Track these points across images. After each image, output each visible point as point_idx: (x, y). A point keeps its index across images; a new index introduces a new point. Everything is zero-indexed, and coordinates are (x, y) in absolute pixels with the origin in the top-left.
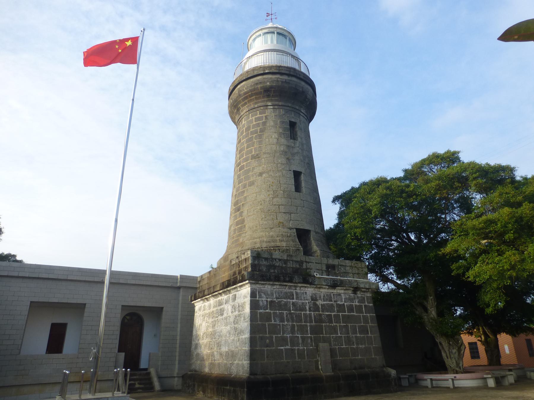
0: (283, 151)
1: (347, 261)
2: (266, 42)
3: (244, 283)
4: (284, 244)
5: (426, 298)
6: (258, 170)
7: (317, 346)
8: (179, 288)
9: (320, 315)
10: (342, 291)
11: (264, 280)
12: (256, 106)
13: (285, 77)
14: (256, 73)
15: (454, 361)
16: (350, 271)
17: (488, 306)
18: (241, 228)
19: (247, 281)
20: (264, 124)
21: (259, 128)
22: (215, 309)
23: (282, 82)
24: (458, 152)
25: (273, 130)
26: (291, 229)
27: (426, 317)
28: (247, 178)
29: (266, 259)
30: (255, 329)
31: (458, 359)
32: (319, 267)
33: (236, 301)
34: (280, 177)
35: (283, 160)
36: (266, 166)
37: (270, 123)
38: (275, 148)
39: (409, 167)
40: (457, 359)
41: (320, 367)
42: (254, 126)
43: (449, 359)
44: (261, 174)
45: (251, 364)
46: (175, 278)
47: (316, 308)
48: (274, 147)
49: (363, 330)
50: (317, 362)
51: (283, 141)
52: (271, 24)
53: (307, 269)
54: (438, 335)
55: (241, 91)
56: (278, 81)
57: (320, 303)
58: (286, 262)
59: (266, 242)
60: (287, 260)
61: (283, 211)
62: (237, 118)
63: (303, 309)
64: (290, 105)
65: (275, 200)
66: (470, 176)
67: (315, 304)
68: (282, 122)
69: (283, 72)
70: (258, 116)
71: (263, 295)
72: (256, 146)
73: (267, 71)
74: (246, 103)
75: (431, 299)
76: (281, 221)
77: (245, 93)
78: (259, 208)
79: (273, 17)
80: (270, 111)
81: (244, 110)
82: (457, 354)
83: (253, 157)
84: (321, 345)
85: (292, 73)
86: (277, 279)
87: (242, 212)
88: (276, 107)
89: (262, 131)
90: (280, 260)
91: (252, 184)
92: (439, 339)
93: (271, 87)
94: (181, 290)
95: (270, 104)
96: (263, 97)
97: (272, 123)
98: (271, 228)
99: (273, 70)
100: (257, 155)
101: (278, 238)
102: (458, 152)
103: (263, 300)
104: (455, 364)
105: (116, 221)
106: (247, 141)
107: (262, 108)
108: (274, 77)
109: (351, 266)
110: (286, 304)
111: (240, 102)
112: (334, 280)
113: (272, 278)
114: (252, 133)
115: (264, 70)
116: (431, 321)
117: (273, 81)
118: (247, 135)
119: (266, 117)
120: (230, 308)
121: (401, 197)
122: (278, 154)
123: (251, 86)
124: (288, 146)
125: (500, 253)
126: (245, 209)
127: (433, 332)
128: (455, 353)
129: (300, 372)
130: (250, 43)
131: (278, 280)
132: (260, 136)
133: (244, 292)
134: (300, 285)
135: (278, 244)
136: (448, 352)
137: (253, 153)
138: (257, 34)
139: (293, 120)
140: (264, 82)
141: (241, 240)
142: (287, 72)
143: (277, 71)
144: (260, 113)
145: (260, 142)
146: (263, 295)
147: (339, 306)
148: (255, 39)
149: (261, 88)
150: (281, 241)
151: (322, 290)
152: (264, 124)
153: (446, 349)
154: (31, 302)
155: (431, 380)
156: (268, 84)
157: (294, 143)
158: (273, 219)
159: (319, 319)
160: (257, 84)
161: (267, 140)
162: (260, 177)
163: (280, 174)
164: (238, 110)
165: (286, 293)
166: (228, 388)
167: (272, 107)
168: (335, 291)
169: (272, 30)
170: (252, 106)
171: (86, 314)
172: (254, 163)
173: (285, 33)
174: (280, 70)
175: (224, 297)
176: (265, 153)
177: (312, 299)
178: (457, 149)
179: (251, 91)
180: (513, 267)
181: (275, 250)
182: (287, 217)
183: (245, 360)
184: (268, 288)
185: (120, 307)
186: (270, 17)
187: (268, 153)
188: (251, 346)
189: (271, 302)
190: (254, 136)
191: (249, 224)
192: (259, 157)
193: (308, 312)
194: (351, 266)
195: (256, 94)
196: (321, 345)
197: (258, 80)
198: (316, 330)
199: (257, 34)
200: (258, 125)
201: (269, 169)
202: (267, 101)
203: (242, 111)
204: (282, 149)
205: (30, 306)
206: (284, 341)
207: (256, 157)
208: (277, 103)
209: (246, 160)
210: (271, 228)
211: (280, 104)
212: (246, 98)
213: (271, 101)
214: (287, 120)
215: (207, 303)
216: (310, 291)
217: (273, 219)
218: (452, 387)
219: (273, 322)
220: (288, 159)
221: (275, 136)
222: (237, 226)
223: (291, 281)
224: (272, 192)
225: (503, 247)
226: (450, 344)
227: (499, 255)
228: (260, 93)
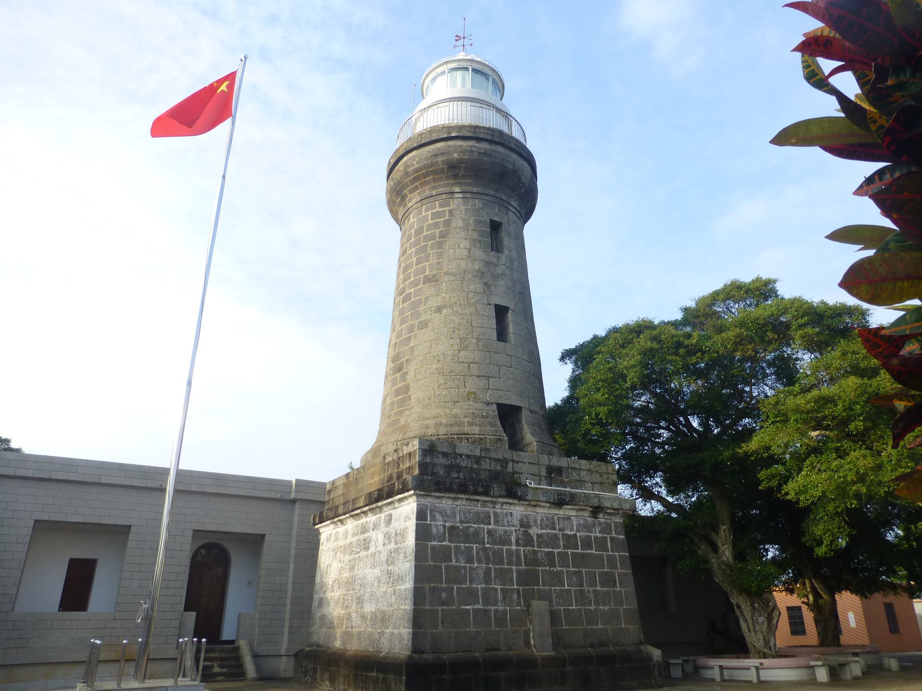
0: (478, 271)
1: (583, 462)
2: (454, 84)
3: (406, 494)
4: (476, 430)
6: (434, 303)
7: (528, 605)
8: (293, 501)
9: (535, 552)
10: (574, 513)
11: (440, 491)
12: (434, 193)
13: (484, 146)
14: (435, 136)
16: (588, 478)
17: (820, 543)
18: (402, 403)
19: (412, 492)
20: (447, 223)
21: (438, 231)
22: (355, 539)
23: (480, 153)
24: (775, 281)
25: (462, 234)
26: (488, 404)
28: (416, 315)
29: (445, 455)
32: (534, 469)
33: (392, 526)
34: (471, 314)
35: (477, 286)
36: (448, 296)
37: (458, 222)
38: (464, 266)
39: (692, 304)
41: (532, 642)
42: (430, 227)
44: (439, 309)
45: (414, 634)
47: (527, 540)
48: (463, 264)
49: (608, 580)
50: (527, 633)
51: (478, 253)
52: (463, 53)
53: (514, 473)
55: (409, 166)
56: (471, 151)
57: (534, 531)
58: (478, 460)
59: (446, 426)
60: (481, 457)
61: (476, 373)
64: (492, 192)
65: (462, 354)
66: (794, 323)
67: (526, 534)
68: (478, 222)
69: (481, 136)
70: (437, 209)
71: (438, 516)
73: (453, 135)
74: (416, 188)
76: (473, 390)
77: (416, 171)
78: (434, 366)
79: (467, 42)
81: (414, 199)
83: (427, 280)
84: (535, 603)
85: (496, 139)
86: (462, 489)
87: (406, 373)
88: (468, 195)
89: (443, 235)
90: (468, 457)
91: (423, 325)
93: (461, 161)
94: (297, 505)
95: (457, 190)
96: (447, 178)
97: (460, 223)
100: (434, 276)
101: (466, 420)
102: (775, 281)
103: (438, 525)
104: (762, 641)
105: (189, 383)
107: (444, 196)
109: (589, 471)
111: (406, 185)
112: (560, 494)
113: (455, 486)
114: (426, 239)
115: (449, 133)
117: (463, 152)
118: (417, 242)
119: (450, 211)
120: (380, 537)
123: (427, 158)
124: (487, 263)
125: (841, 454)
126: (411, 369)
129: (498, 649)
131: (465, 492)
132: (440, 245)
133: (406, 510)
134: (501, 500)
135: (467, 429)
137: (427, 273)
139: (496, 219)
140: (449, 153)
141: (403, 421)
142: (489, 137)
143: (471, 135)
144: (441, 206)
145: (440, 255)
146: (438, 516)
148: (434, 79)
149: (444, 162)
150: (471, 424)
152: (447, 223)
154: (36, 521)
155: (721, 668)
156: (456, 155)
157: (498, 258)
159: (533, 560)
160: (436, 155)
161: (451, 251)
162: (437, 315)
163: (472, 309)
164: (403, 198)
165: (478, 513)
166: (374, 674)
167: (460, 195)
168: (561, 512)
169: (464, 64)
171: (130, 544)
172: (429, 290)
173: (486, 70)
174: (476, 132)
175: (371, 518)
176: (446, 274)
177: (522, 525)
179: (426, 166)
180: (861, 478)
181: (461, 439)
182: (482, 383)
183: (404, 628)
184: (446, 503)
185: (190, 533)
186: (461, 42)
187: (452, 274)
188: (415, 603)
189: (452, 528)
190: (429, 243)
191: (417, 393)
192: (436, 281)
193: (514, 547)
194: (589, 471)
195: (435, 172)
196: (535, 603)
197: (439, 149)
198: (528, 578)
200: (436, 225)
201: (453, 301)
202: (453, 185)
203: (410, 201)
204: (477, 267)
205: (193, 537)
206: (471, 595)
208: (470, 189)
209: (415, 284)
212: (416, 179)
213: (460, 184)
214: (486, 218)
215: (341, 529)
216: (518, 510)
217: (458, 387)
218: (755, 680)
219: (454, 563)
220: (486, 284)
221: (465, 244)
222: (396, 396)
223: (486, 493)
224: (458, 341)
225: (846, 444)
227: (840, 457)
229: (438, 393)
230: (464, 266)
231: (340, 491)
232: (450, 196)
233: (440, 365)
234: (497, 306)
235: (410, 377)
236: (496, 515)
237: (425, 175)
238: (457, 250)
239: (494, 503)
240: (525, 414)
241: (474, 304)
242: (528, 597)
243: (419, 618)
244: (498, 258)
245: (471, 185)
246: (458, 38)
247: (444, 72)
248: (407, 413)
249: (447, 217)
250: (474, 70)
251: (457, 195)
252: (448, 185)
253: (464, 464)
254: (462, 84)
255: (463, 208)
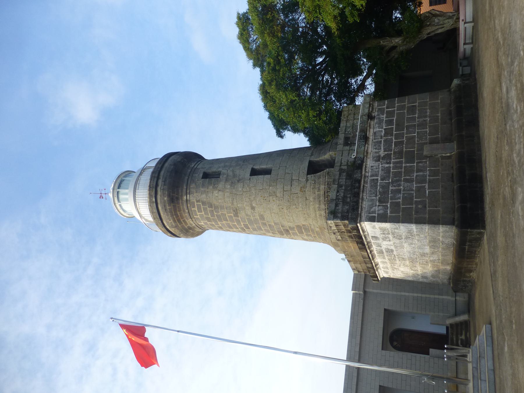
1: (342, 125)
2: (127, 200)
3: (360, 228)
5: (382, 48)
6: (249, 211)
7: (426, 157)
8: (365, 292)
9: (395, 153)
10: (372, 130)
12: (187, 211)
13: (160, 182)
15: (447, 21)
16: (351, 122)
18: (307, 230)
19: (358, 225)
20: (204, 203)
23: (164, 185)
24: (238, 14)
25: (210, 195)
26: (307, 180)
27: (401, 48)
29: (337, 205)
30: (407, 219)
31: (444, 17)
32: (345, 153)
33: (379, 236)
34: (255, 190)
35: (240, 186)
36: (245, 203)
37: (203, 197)
38: (228, 194)
39: (251, 62)
40: (445, 18)
41: (448, 155)
42: (206, 213)
43: (445, 25)
44: (253, 208)
45: (443, 224)
46: (355, 297)
47: (387, 158)
48: (227, 194)
49: (412, 110)
50: (443, 158)
51: (221, 185)
53: (347, 165)
54: (419, 36)
56: (163, 189)
57: (382, 153)
58: (340, 186)
59: (320, 204)
60: (338, 184)
61: (289, 187)
62: (198, 230)
63: (388, 170)
64: (186, 178)
65: (278, 195)
67: (384, 158)
68: (203, 185)
69: (155, 184)
70: (196, 209)
71: (372, 210)
72: (225, 212)
73: (154, 200)
74: (184, 221)
75: (383, 42)
76: (299, 189)
77: (174, 221)
79: (103, 192)
80: (192, 198)
81: (190, 222)
82: (439, 18)
83: (236, 215)
85: (156, 175)
86: (357, 195)
87: (290, 227)
88: (188, 191)
89: (211, 206)
90: (338, 192)
91: (262, 217)
92: (424, 35)
93: (169, 196)
94: (367, 290)
95: (185, 197)
96: (178, 203)
97: (204, 196)
98: (306, 199)
99: (153, 193)
100: (234, 211)
101: (317, 193)
102: (238, 14)
103: (378, 209)
104: (450, 20)
106: (220, 220)
107: (189, 205)
108: (159, 193)
110: (382, 187)
111: (183, 226)
112: (360, 138)
113: (355, 200)
114: (213, 215)
115: (153, 202)
116: (405, 43)
117: (164, 194)
119: (198, 201)
121: (279, 71)
122: (234, 190)
123: (167, 215)
124: (227, 180)
126: (287, 224)
127: (417, 41)
128: (439, 19)
129: (453, 174)
130: (128, 216)
131: (358, 194)
132: (216, 208)
133: (369, 228)
134: (363, 173)
135: (322, 193)
136: (437, 27)
138: (119, 208)
139: (201, 175)
140: (164, 202)
141: (318, 229)
143: (154, 190)
144: (194, 207)
145: (222, 208)
146: (372, 210)
147: (386, 134)
149: (169, 205)
150: (319, 190)
151: (370, 151)
152: (204, 203)
153: (434, 28)
156: (166, 199)
157: (224, 174)
158: (298, 197)
159: (399, 154)
160: (166, 210)
161: (220, 201)
163: (253, 189)
164: (190, 228)
166: (467, 247)
167: (188, 196)
170: (187, 215)
172: (242, 214)
173: (119, 181)
175: (374, 248)
176: (232, 204)
177: (379, 160)
178: (235, 16)
179: (172, 215)
181: (328, 196)
182: (295, 183)
183: (439, 230)
185: (384, 352)
186: (104, 195)
187: (232, 201)
188: (425, 223)
189: (380, 201)
190: (215, 213)
191: (302, 222)
193: (392, 165)
195: (175, 210)
196: (425, 153)
199: (119, 208)
200: (205, 209)
202: (182, 200)
203: (191, 225)
204: (229, 186)
207: (236, 212)
208: (184, 190)
209: (238, 222)
210: (306, 199)
211: (185, 187)
212: (179, 221)
213: (182, 196)
214: (201, 181)
215: (381, 265)
216: (370, 162)
217: (298, 197)
218: (472, 24)
219: (401, 200)
220: (238, 181)
221: (216, 193)
223: (359, 182)
224: (271, 197)
226: (429, 25)
228: (174, 206)
229: (301, 209)
230: (228, 194)
231: (359, 266)
232: (188, 203)
233: (285, 208)
234: (251, 175)
235: (291, 225)
236: (372, 176)
237: (177, 216)
238: (219, 197)
239: (365, 176)
240: (313, 159)
241: (250, 188)
242: (421, 157)
243: (433, 221)
244: (224, 174)
245: (182, 191)
246: (101, 197)
247: (120, 205)
248: (313, 227)
249: (201, 204)
250: (119, 188)
251: (188, 198)
252: (183, 204)
253: (342, 194)
254: (126, 195)
255: (195, 194)
